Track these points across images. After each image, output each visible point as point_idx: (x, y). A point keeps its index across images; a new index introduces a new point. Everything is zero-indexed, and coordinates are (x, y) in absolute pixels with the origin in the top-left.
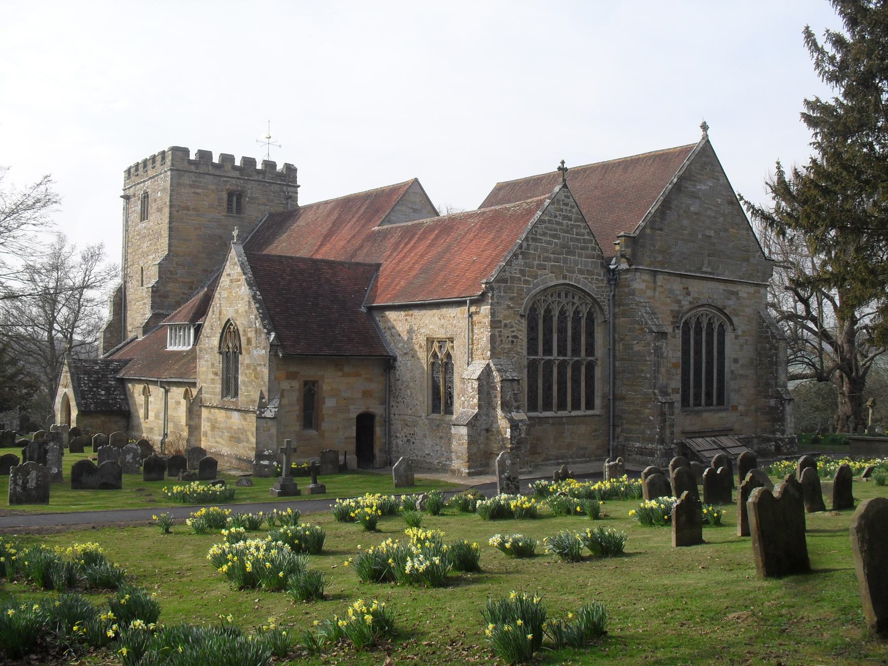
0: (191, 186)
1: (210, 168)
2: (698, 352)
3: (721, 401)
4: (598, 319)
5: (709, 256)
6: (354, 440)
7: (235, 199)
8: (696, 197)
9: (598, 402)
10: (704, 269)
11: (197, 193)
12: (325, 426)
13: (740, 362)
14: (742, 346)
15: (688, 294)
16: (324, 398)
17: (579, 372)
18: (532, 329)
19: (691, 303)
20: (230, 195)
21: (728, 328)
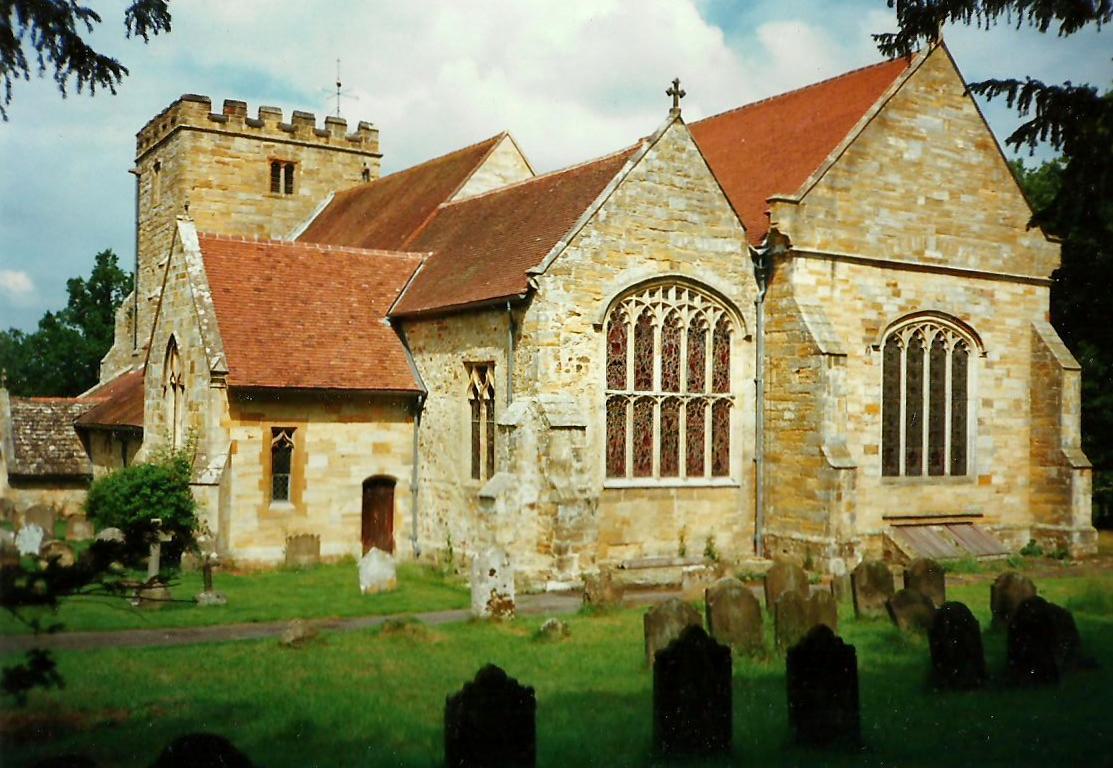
0: (213, 153)
1: (244, 126)
2: (914, 390)
3: (959, 467)
4: (737, 335)
5: (938, 232)
6: (359, 519)
7: (282, 171)
8: (917, 138)
9: (735, 463)
10: (928, 253)
11: (224, 163)
12: (307, 496)
13: (997, 405)
14: (998, 379)
15: (897, 294)
16: (307, 455)
17: (701, 416)
18: (616, 346)
19: (901, 309)
20: (276, 165)
21: (974, 352)
